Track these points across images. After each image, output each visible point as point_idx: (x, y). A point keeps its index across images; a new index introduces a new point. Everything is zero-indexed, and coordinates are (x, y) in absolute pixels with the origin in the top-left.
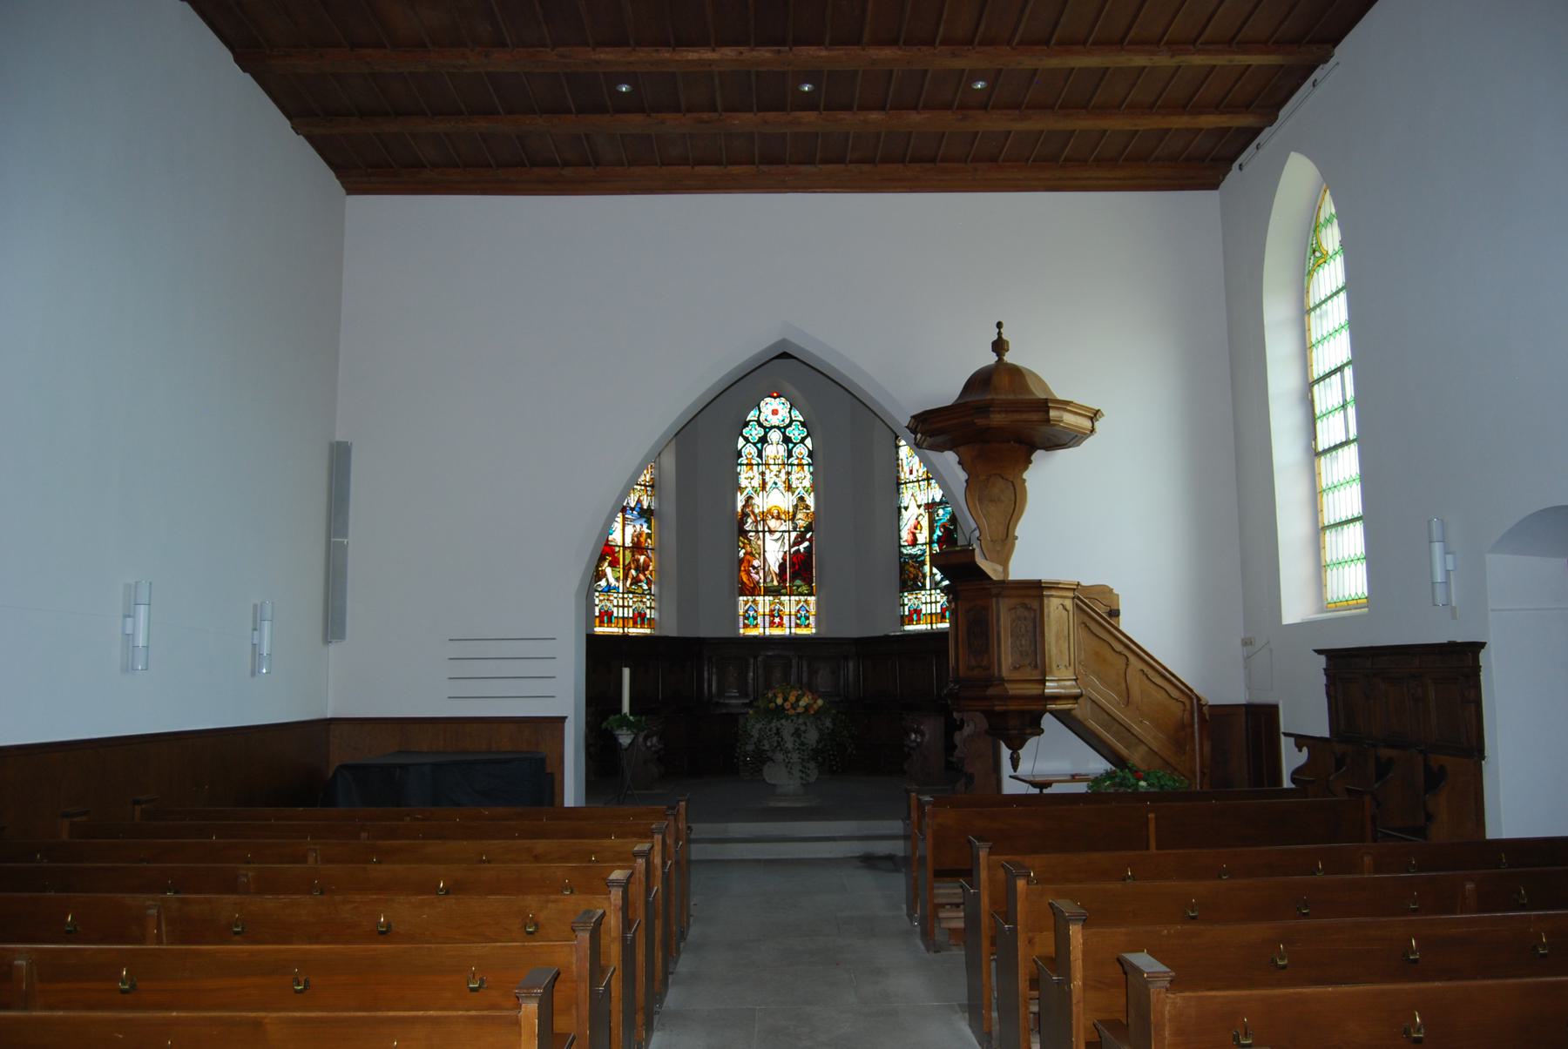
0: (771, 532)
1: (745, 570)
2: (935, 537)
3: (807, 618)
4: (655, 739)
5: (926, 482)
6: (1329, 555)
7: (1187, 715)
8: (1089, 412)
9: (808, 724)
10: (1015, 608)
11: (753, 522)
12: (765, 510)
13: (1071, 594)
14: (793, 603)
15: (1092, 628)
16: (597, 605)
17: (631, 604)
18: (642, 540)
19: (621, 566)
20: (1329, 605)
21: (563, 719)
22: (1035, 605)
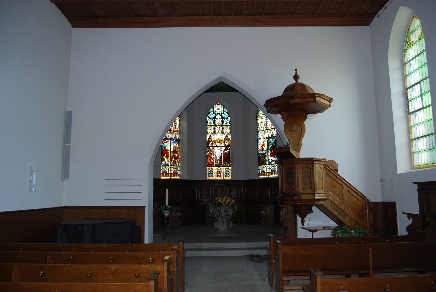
0: (217, 147)
1: (209, 159)
2: (269, 148)
3: (229, 174)
4: (179, 213)
5: (266, 130)
6: (414, 149)
7: (364, 206)
8: (329, 99)
9: (229, 208)
10: (304, 168)
11: (212, 144)
12: (215, 140)
13: (323, 163)
14: (224, 169)
15: (330, 175)
16: (162, 170)
17: (173, 169)
18: (176, 149)
19: (170, 157)
20: (415, 167)
21: (144, 207)
22: (311, 166)
